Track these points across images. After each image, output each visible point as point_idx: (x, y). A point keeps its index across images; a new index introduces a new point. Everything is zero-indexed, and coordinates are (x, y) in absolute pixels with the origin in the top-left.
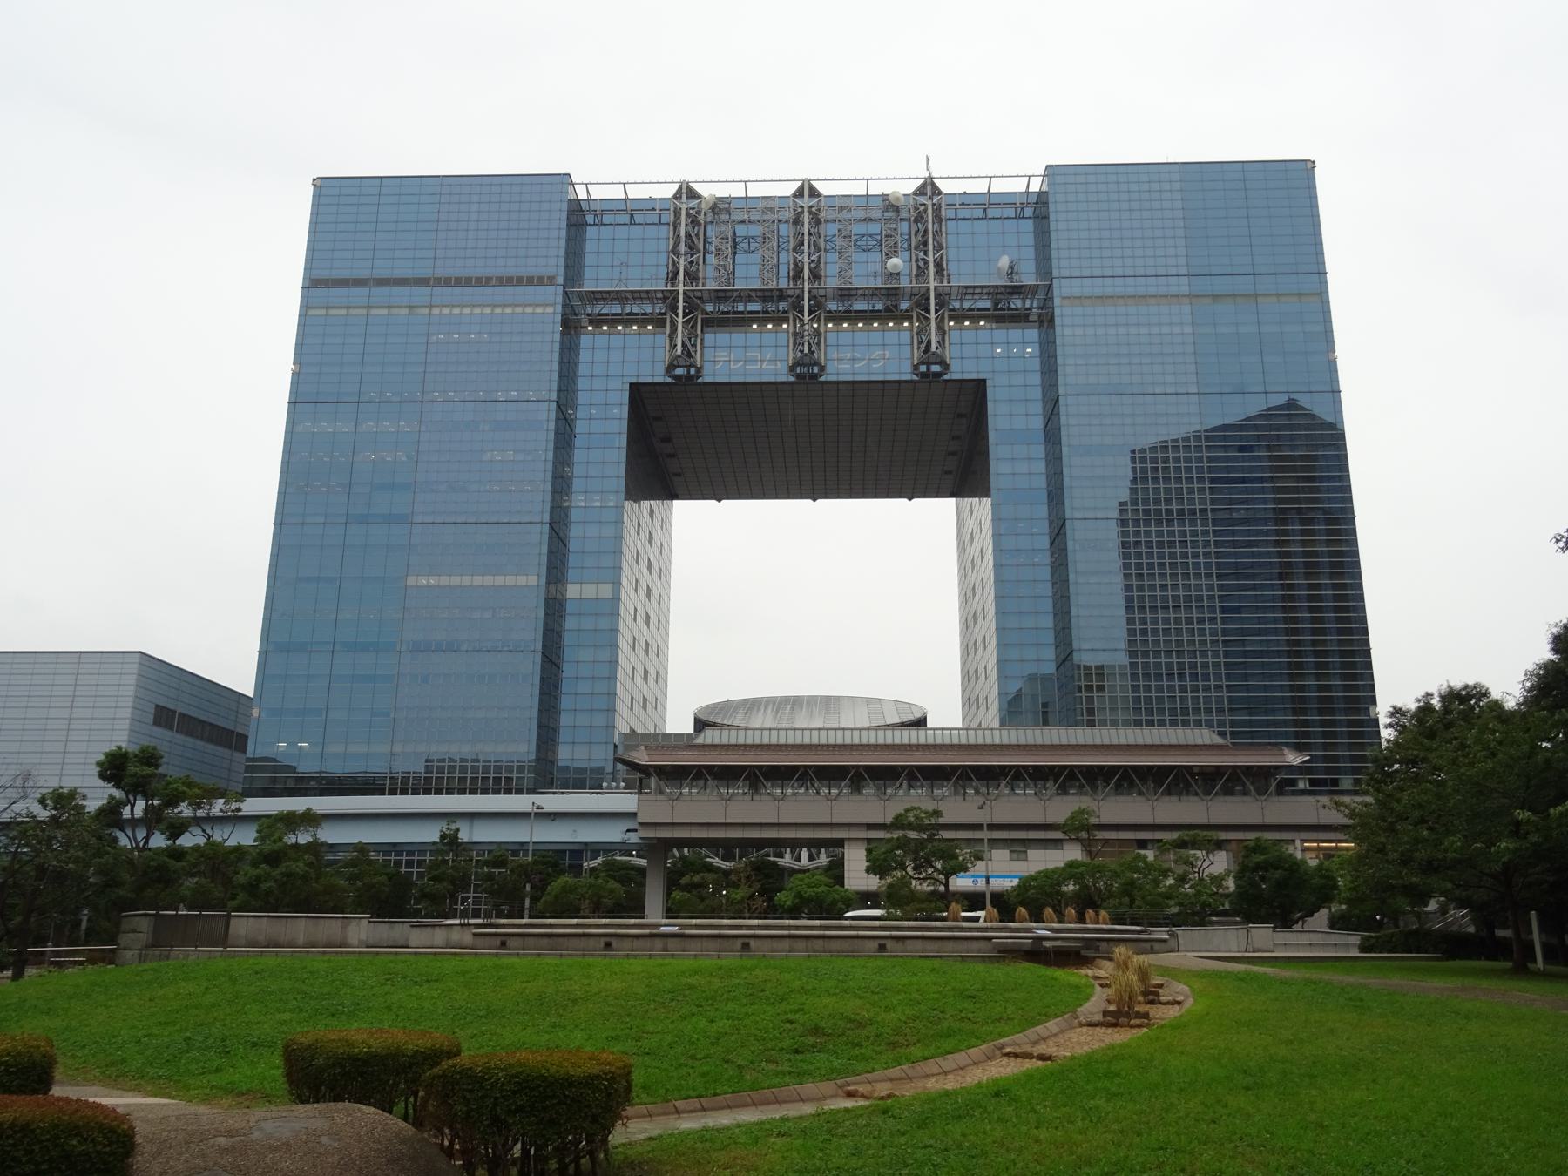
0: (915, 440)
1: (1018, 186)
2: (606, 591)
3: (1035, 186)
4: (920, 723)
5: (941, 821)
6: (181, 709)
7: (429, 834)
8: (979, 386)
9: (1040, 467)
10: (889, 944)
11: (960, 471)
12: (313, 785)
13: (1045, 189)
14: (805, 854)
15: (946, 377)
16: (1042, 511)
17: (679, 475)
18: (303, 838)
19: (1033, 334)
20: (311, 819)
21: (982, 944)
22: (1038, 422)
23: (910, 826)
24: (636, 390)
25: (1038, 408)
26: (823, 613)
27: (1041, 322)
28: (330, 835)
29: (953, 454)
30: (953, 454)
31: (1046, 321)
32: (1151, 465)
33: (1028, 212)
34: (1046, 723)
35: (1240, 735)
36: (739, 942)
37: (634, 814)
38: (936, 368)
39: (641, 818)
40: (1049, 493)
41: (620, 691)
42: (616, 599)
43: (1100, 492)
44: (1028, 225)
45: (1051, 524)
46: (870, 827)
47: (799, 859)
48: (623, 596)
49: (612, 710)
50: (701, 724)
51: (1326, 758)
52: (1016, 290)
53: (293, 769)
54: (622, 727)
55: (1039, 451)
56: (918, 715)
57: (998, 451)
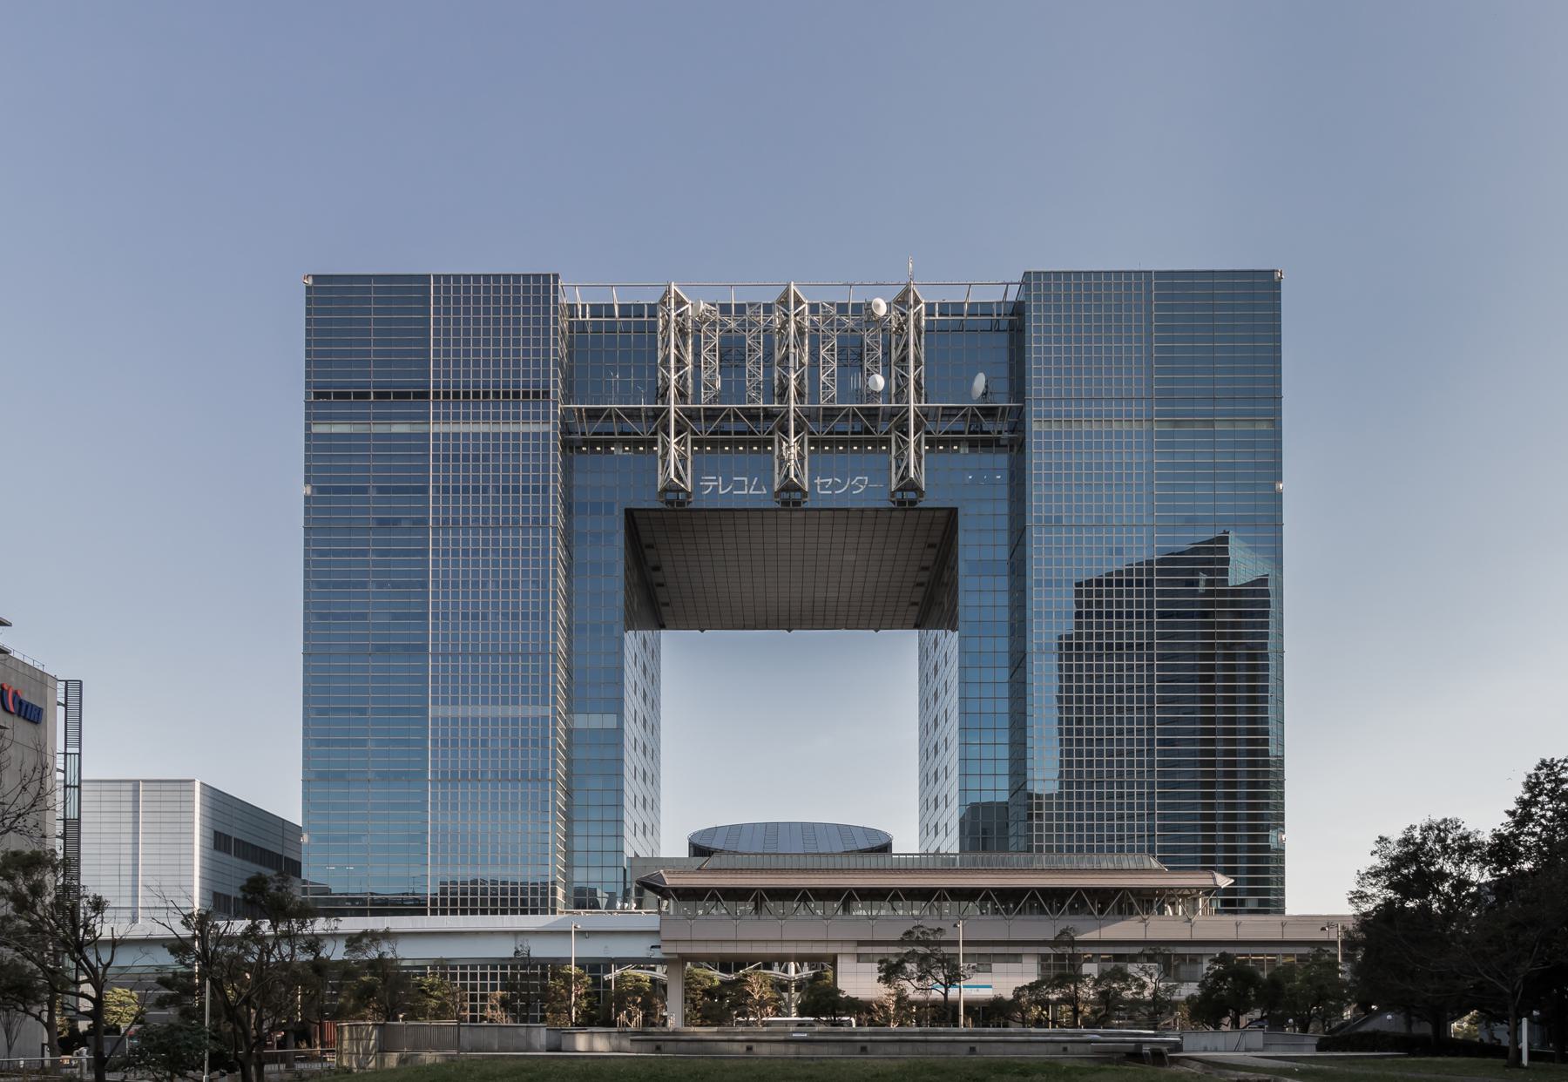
0: (914, 575)
1: (994, 296)
2: (610, 721)
3: (1012, 297)
4: (885, 848)
5: (944, 938)
6: (235, 834)
7: (505, 950)
8: (952, 513)
9: (1004, 599)
10: (869, 1046)
11: (928, 601)
12: (348, 905)
13: (1022, 298)
14: (792, 966)
15: (919, 505)
16: (1003, 645)
17: (667, 604)
18: (373, 954)
19: (1002, 460)
20: (387, 935)
21: (1052, 1047)
22: (1003, 554)
23: (919, 942)
24: (630, 513)
25: (1004, 538)
26: (807, 748)
27: (1012, 447)
28: (408, 953)
29: (921, 584)
30: (921, 584)
31: (1017, 446)
32: (1095, 596)
33: (1004, 325)
34: (984, 849)
35: (1172, 860)
36: (859, 1045)
37: (658, 932)
38: (911, 495)
39: (664, 937)
40: (1012, 626)
41: (626, 818)
42: (620, 730)
43: (1051, 618)
44: (1003, 339)
45: (1011, 656)
46: (861, 943)
47: (786, 971)
48: (626, 726)
49: (619, 836)
50: (698, 850)
51: (1250, 881)
52: (990, 413)
53: (327, 891)
54: (629, 853)
55: (1003, 583)
56: (884, 841)
57: (966, 581)
